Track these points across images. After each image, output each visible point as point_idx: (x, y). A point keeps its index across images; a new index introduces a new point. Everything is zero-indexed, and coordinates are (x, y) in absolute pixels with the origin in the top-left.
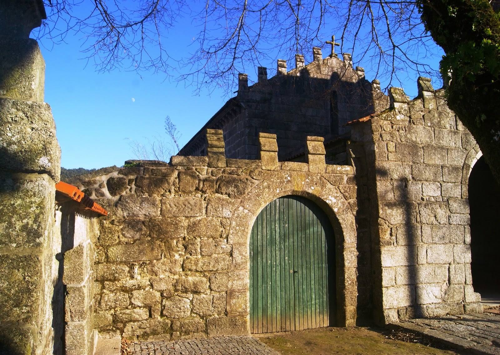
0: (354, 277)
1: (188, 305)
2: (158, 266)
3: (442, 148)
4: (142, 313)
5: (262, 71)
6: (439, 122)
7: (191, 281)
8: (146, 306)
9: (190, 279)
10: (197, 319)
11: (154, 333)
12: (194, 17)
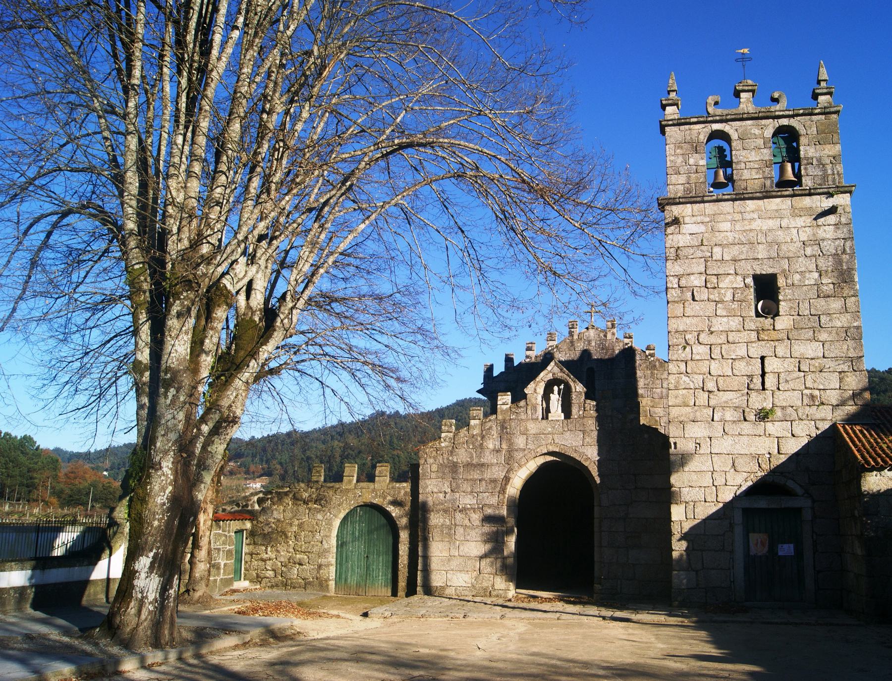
0: (406, 562)
1: (296, 572)
2: (280, 548)
3: (483, 465)
4: (270, 574)
5: (509, 360)
6: (482, 444)
7: (526, 628)
8: (273, 570)
9: (298, 556)
10: (300, 580)
11: (277, 585)
12: (716, 127)
